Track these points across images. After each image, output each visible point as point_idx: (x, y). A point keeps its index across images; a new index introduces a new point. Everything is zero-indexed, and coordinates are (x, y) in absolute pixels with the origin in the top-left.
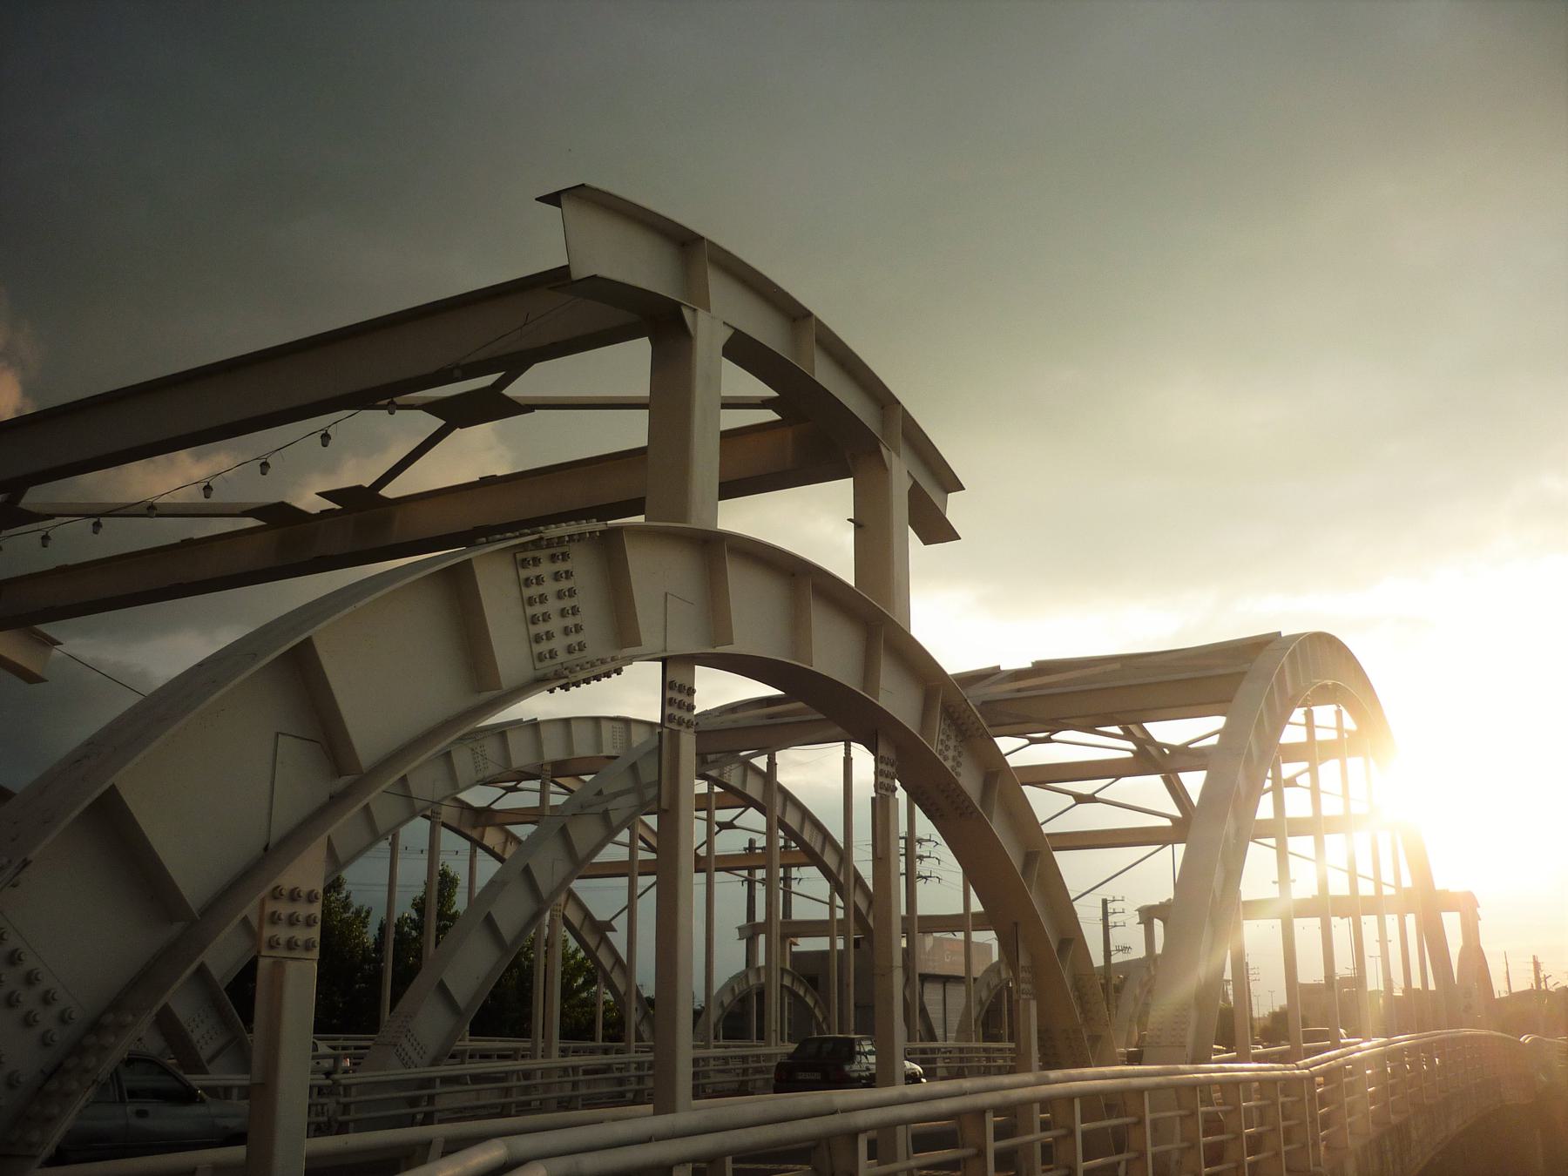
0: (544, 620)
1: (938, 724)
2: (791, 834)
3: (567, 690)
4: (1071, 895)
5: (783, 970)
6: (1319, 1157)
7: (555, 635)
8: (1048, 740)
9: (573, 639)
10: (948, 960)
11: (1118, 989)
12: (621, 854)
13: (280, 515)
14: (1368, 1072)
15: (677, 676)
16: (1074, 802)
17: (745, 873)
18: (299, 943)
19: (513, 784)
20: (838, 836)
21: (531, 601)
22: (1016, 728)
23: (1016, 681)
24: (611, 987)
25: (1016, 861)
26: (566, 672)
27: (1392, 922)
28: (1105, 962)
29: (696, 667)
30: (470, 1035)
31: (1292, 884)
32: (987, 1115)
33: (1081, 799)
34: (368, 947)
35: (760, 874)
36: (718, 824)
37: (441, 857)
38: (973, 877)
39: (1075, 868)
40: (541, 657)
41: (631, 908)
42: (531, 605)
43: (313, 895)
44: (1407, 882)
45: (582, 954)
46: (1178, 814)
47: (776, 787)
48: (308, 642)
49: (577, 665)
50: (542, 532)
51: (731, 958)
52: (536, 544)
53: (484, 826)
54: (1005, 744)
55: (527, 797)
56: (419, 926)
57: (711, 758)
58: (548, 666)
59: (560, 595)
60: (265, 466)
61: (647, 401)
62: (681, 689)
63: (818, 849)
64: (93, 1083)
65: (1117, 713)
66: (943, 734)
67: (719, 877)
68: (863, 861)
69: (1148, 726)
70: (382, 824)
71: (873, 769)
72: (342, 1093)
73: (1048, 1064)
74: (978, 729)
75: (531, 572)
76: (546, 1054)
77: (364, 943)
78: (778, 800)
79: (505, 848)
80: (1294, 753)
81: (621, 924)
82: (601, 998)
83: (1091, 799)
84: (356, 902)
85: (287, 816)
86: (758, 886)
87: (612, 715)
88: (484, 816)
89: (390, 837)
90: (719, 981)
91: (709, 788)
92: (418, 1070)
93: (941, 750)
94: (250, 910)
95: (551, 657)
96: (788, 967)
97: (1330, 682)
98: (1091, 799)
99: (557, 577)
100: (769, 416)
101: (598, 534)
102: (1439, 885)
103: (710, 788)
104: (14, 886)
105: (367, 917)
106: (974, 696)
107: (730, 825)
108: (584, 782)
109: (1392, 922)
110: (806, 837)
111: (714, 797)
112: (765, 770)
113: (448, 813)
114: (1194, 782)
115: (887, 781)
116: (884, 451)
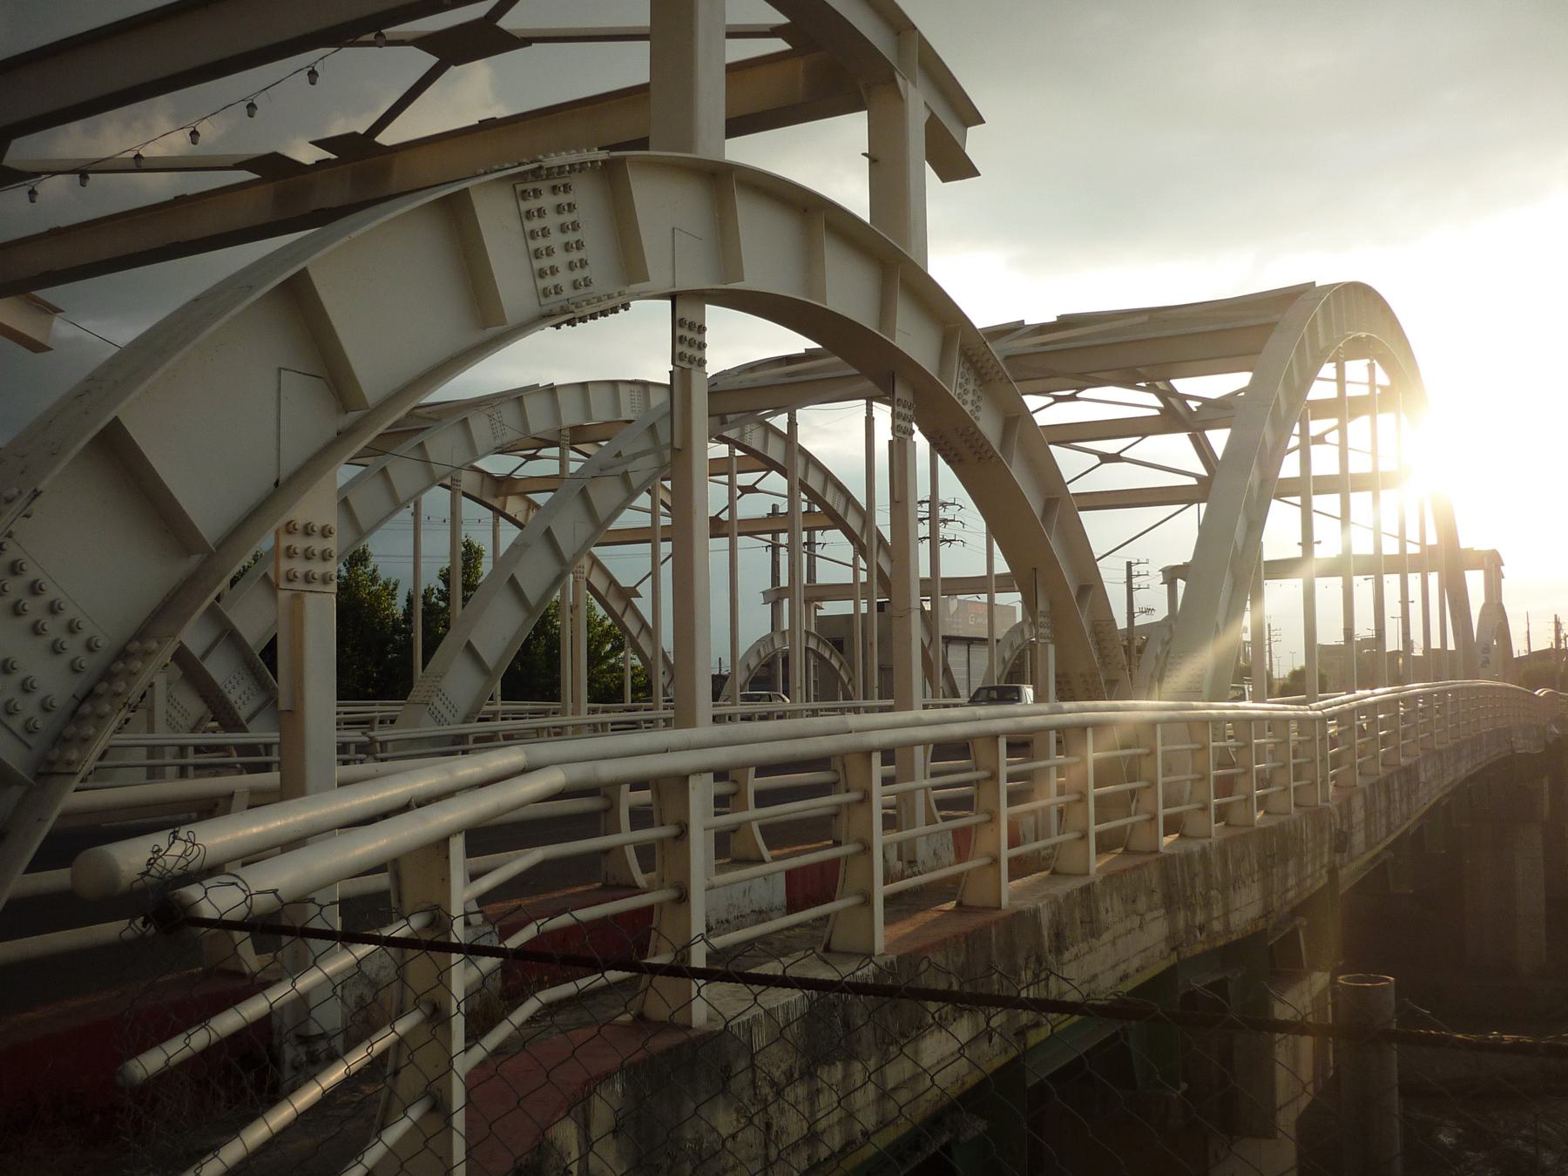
0: (548, 255)
1: (956, 366)
2: (814, 497)
3: (574, 325)
4: (1095, 555)
5: (808, 633)
6: (1328, 795)
7: (559, 269)
8: (1073, 398)
9: (579, 274)
10: (972, 623)
11: (1140, 650)
12: (644, 520)
13: (274, 167)
14: (1381, 716)
15: (686, 312)
16: (1099, 462)
17: (769, 537)
18: (316, 576)
19: (533, 451)
20: (861, 498)
21: (533, 235)
22: (1041, 384)
23: (1041, 334)
24: (638, 651)
25: (1036, 507)
26: (572, 307)
27: (1414, 580)
28: (1128, 625)
29: (708, 307)
30: (502, 700)
31: (1316, 545)
32: (1000, 739)
33: (1106, 458)
34: (398, 619)
35: (783, 538)
36: (740, 488)
37: (463, 527)
38: (998, 529)
39: (1100, 528)
40: (546, 292)
41: (654, 574)
42: (525, 200)
43: (327, 530)
44: (1432, 540)
45: (609, 621)
46: (1204, 472)
47: (797, 448)
48: (304, 273)
49: (584, 301)
50: (540, 161)
51: (756, 623)
52: (536, 174)
53: (507, 495)
54: (1032, 402)
55: (546, 465)
56: (445, 596)
57: (730, 418)
58: (553, 302)
59: (563, 229)
60: (251, 107)
61: (647, 32)
62: (691, 326)
63: (840, 512)
64: (124, 706)
65: (1139, 367)
66: (962, 378)
67: (743, 541)
68: (883, 520)
69: (1174, 382)
70: (402, 492)
71: (890, 425)
72: (379, 749)
73: (1062, 697)
74: (997, 372)
75: (532, 204)
76: (576, 712)
77: (393, 615)
78: (800, 462)
79: (527, 515)
80: (1323, 409)
81: (645, 589)
82: (629, 664)
83: (1116, 458)
84: (383, 576)
85: (293, 456)
86: (783, 551)
87: (630, 379)
88: (504, 485)
89: (412, 505)
90: (744, 646)
91: (730, 452)
92: (449, 727)
93: (959, 394)
94: (265, 543)
95: (556, 293)
96: (813, 630)
97: (1364, 335)
98: (1116, 458)
99: (559, 209)
100: (779, 45)
101: (600, 163)
102: (1464, 544)
103: (731, 452)
104: (27, 516)
105: (394, 589)
106: (997, 349)
107: (751, 489)
108: (601, 446)
109: (1414, 580)
110: (829, 499)
111: (735, 460)
112: (786, 432)
113: (468, 481)
114: (1218, 439)
115: (904, 424)
116: (900, 80)
